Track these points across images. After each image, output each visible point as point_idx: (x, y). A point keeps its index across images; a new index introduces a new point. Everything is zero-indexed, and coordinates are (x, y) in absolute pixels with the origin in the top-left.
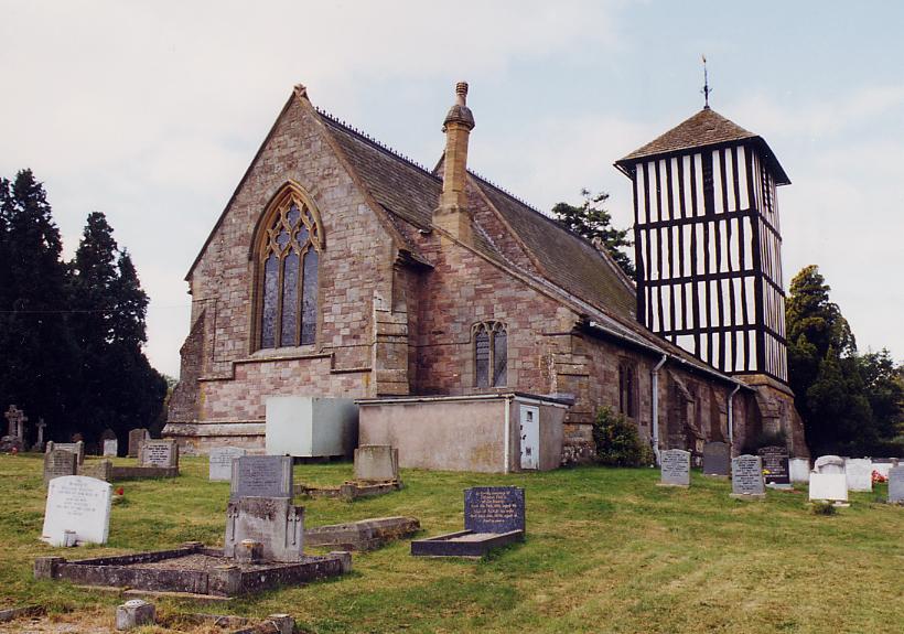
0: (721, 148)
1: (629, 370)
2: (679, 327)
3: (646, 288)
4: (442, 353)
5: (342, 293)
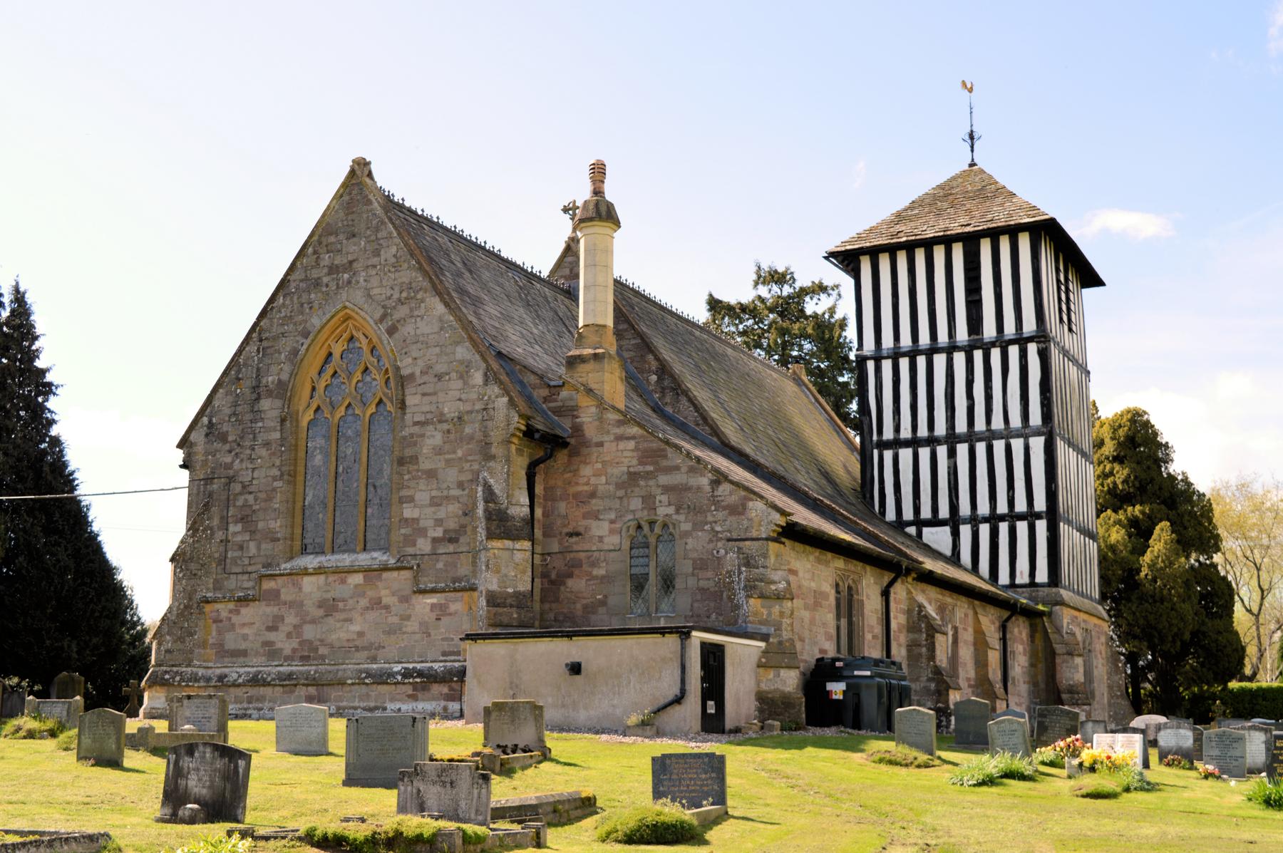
0: (994, 235)
1: (850, 588)
2: (926, 513)
3: (876, 452)
4: (578, 564)
5: (431, 474)
